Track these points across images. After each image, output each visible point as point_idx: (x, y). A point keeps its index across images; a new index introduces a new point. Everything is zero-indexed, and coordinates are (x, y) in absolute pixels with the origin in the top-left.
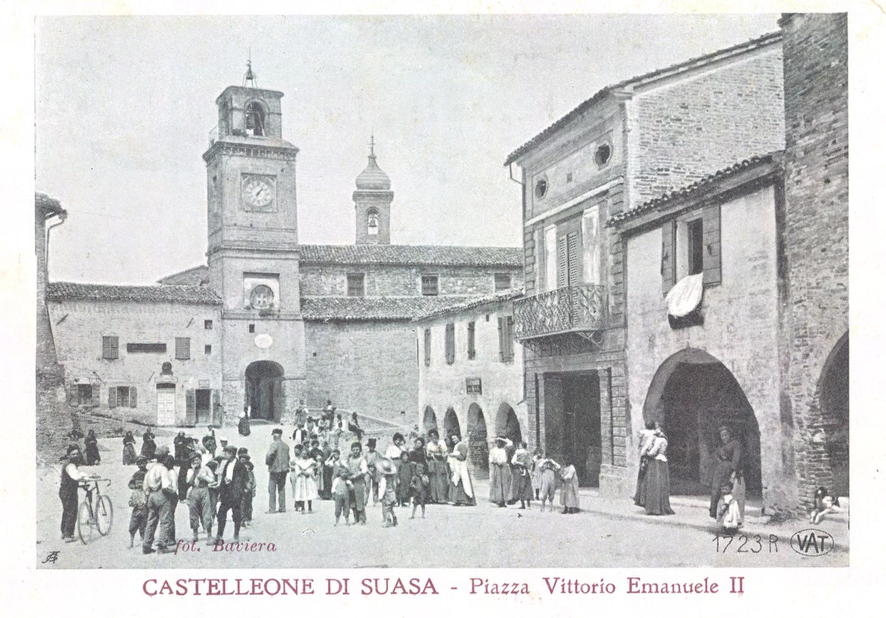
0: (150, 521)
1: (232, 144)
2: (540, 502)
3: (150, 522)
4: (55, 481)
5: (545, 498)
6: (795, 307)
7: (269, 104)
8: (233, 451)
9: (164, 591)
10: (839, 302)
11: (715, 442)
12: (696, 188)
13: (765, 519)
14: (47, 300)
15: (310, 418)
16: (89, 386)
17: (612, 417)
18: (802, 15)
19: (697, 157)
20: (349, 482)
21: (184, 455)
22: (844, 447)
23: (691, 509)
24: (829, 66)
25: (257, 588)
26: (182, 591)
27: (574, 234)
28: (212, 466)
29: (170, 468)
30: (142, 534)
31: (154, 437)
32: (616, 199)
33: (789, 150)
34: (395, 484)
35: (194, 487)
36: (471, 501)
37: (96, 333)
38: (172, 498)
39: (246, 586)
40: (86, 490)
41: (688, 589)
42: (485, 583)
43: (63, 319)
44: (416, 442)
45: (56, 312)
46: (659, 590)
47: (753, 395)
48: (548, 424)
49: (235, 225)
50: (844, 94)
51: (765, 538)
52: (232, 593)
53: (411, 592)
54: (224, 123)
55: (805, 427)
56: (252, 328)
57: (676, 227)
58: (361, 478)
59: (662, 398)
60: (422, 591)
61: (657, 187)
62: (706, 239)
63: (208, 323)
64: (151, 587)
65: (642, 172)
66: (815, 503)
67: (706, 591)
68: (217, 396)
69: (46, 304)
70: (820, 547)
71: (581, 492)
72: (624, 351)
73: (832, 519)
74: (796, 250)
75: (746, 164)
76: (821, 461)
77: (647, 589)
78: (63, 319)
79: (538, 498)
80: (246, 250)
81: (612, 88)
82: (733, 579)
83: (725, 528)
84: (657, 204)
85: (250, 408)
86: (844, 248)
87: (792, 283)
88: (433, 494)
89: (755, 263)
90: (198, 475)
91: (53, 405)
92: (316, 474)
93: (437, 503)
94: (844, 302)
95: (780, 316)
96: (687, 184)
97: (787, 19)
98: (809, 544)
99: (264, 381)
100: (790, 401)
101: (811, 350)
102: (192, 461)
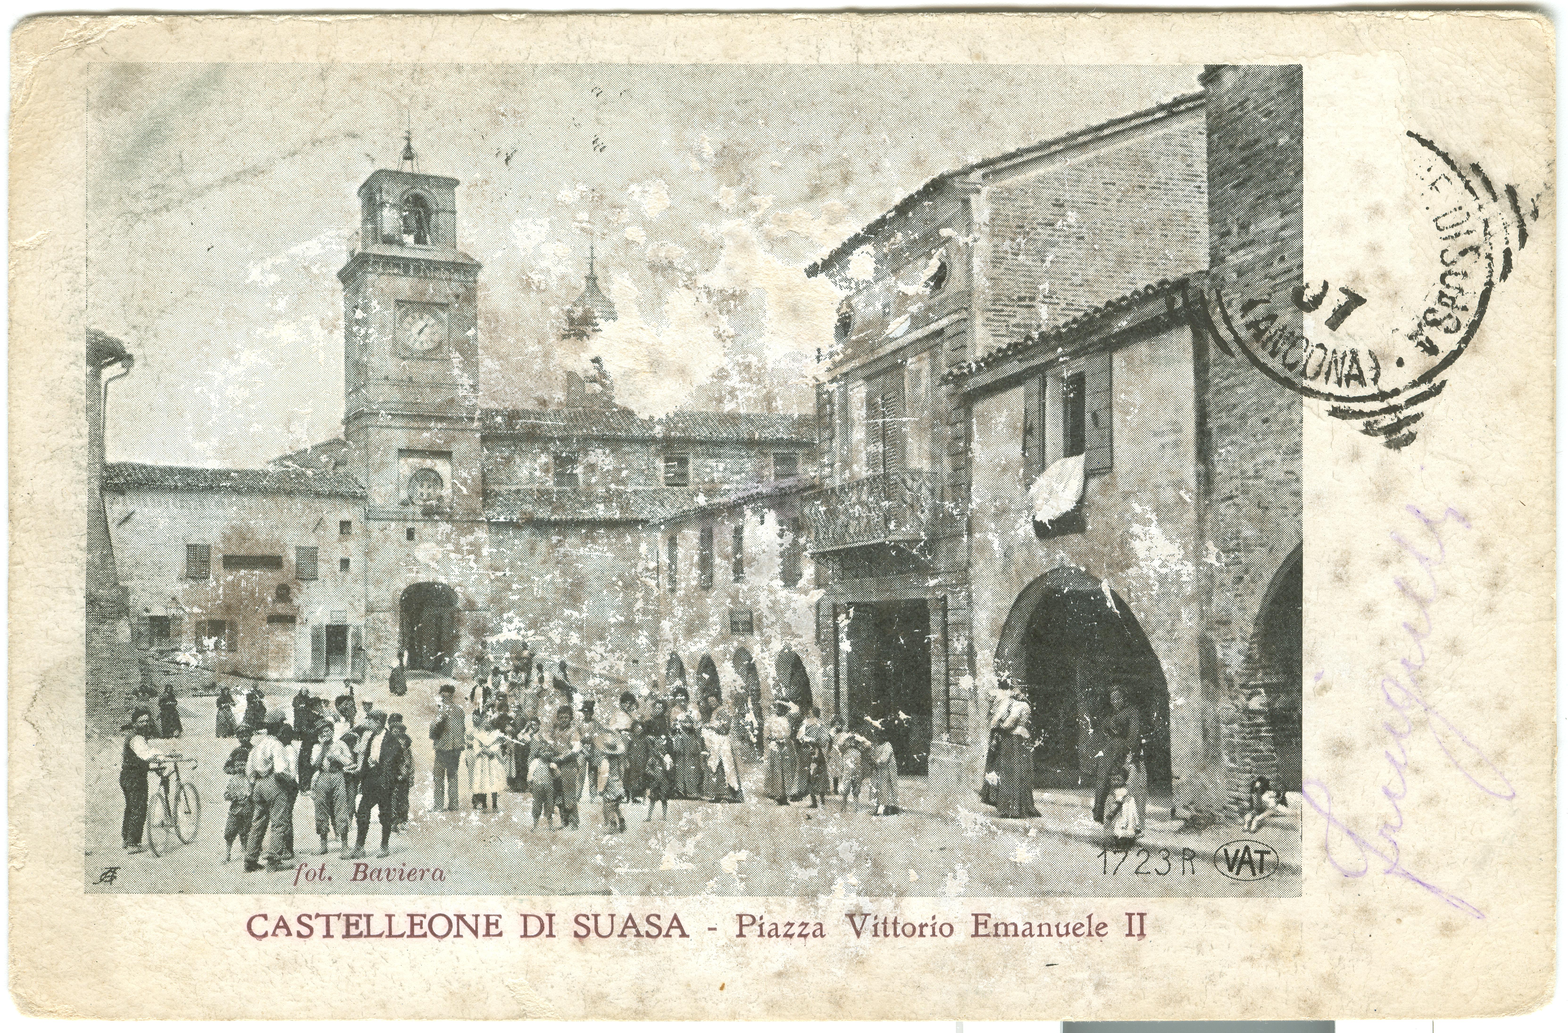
0: (258, 827)
1: (382, 257)
2: (839, 798)
3: (256, 824)
4: (113, 761)
5: (848, 791)
6: (1223, 505)
7: (435, 196)
8: (380, 718)
9: (278, 931)
10: (1288, 499)
11: (1104, 708)
12: (1075, 326)
13: (1177, 824)
14: (103, 489)
15: (496, 669)
16: (165, 618)
17: (948, 670)
18: (1235, 68)
19: (1077, 280)
20: (553, 765)
21: (308, 724)
22: (1295, 716)
23: (1066, 810)
24: (1275, 144)
25: (419, 926)
26: (305, 931)
27: (891, 395)
28: (350, 740)
29: (286, 742)
30: (244, 841)
31: (262, 697)
32: (956, 343)
33: (1214, 270)
34: (622, 769)
35: (322, 771)
36: (735, 796)
37: (176, 539)
38: (289, 789)
39: (401, 925)
40: (160, 774)
41: (1062, 930)
42: (759, 922)
43: (127, 519)
44: (654, 705)
45: (116, 508)
46: (1020, 933)
47: (1159, 639)
48: (851, 681)
49: (386, 378)
50: (1296, 187)
51: (1176, 853)
52: (380, 935)
53: (648, 935)
54: (369, 226)
55: (1237, 687)
56: (410, 534)
57: (1044, 385)
58: (571, 760)
59: (1022, 642)
60: (664, 932)
61: (1017, 325)
62: (1091, 403)
63: (345, 526)
64: (259, 926)
65: (994, 302)
66: (1251, 800)
67: (1090, 934)
68: (357, 636)
69: (102, 495)
70: (1257, 868)
71: (903, 783)
72: (966, 570)
73: (1275, 825)
74: (1225, 420)
75: (1150, 291)
76: (1261, 738)
77: (1001, 929)
78: (127, 519)
79: (836, 792)
80: (403, 416)
81: (951, 176)
82: (1130, 915)
83: (1116, 837)
84: (1017, 350)
85: (406, 654)
86: (1298, 418)
87: (1219, 470)
88: (680, 785)
89: (1164, 440)
90: (329, 754)
91: (112, 646)
92: (504, 753)
93: (686, 798)
94: (1296, 499)
95: (1201, 519)
96: (1061, 321)
97: (1212, 74)
98: (1242, 862)
99: (428, 621)
100: (1214, 648)
101: (1246, 571)
102: (320, 731)
